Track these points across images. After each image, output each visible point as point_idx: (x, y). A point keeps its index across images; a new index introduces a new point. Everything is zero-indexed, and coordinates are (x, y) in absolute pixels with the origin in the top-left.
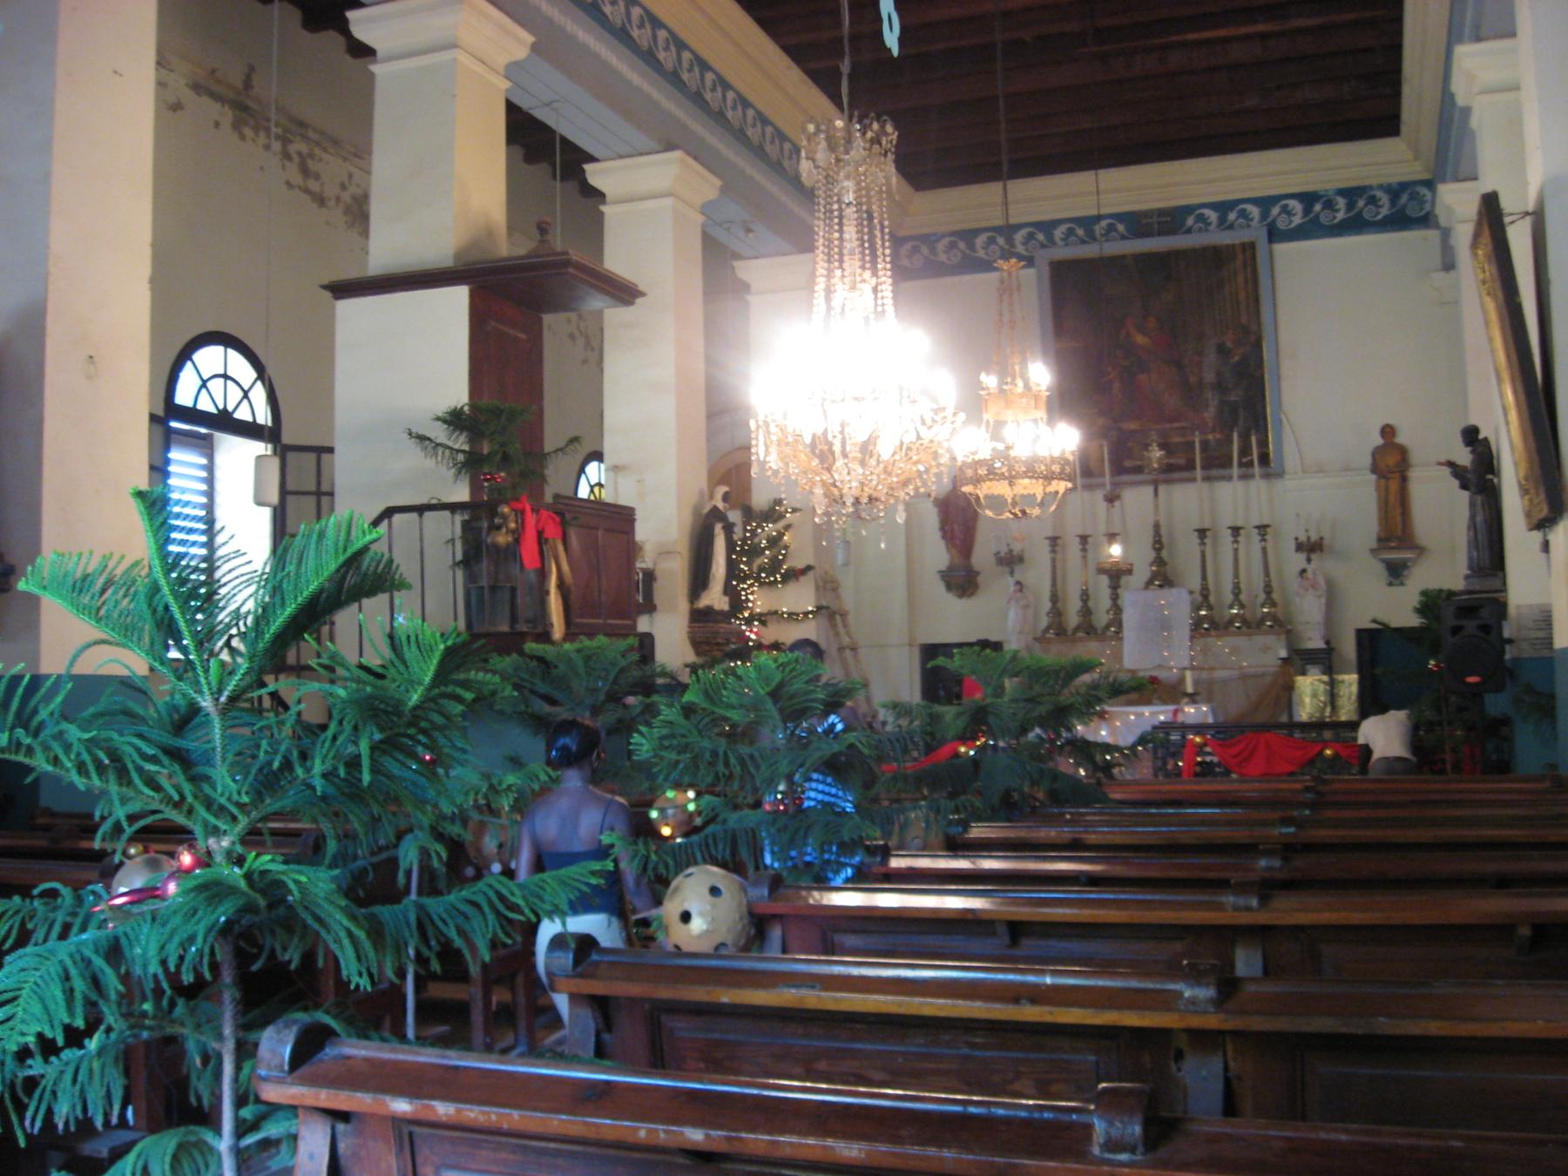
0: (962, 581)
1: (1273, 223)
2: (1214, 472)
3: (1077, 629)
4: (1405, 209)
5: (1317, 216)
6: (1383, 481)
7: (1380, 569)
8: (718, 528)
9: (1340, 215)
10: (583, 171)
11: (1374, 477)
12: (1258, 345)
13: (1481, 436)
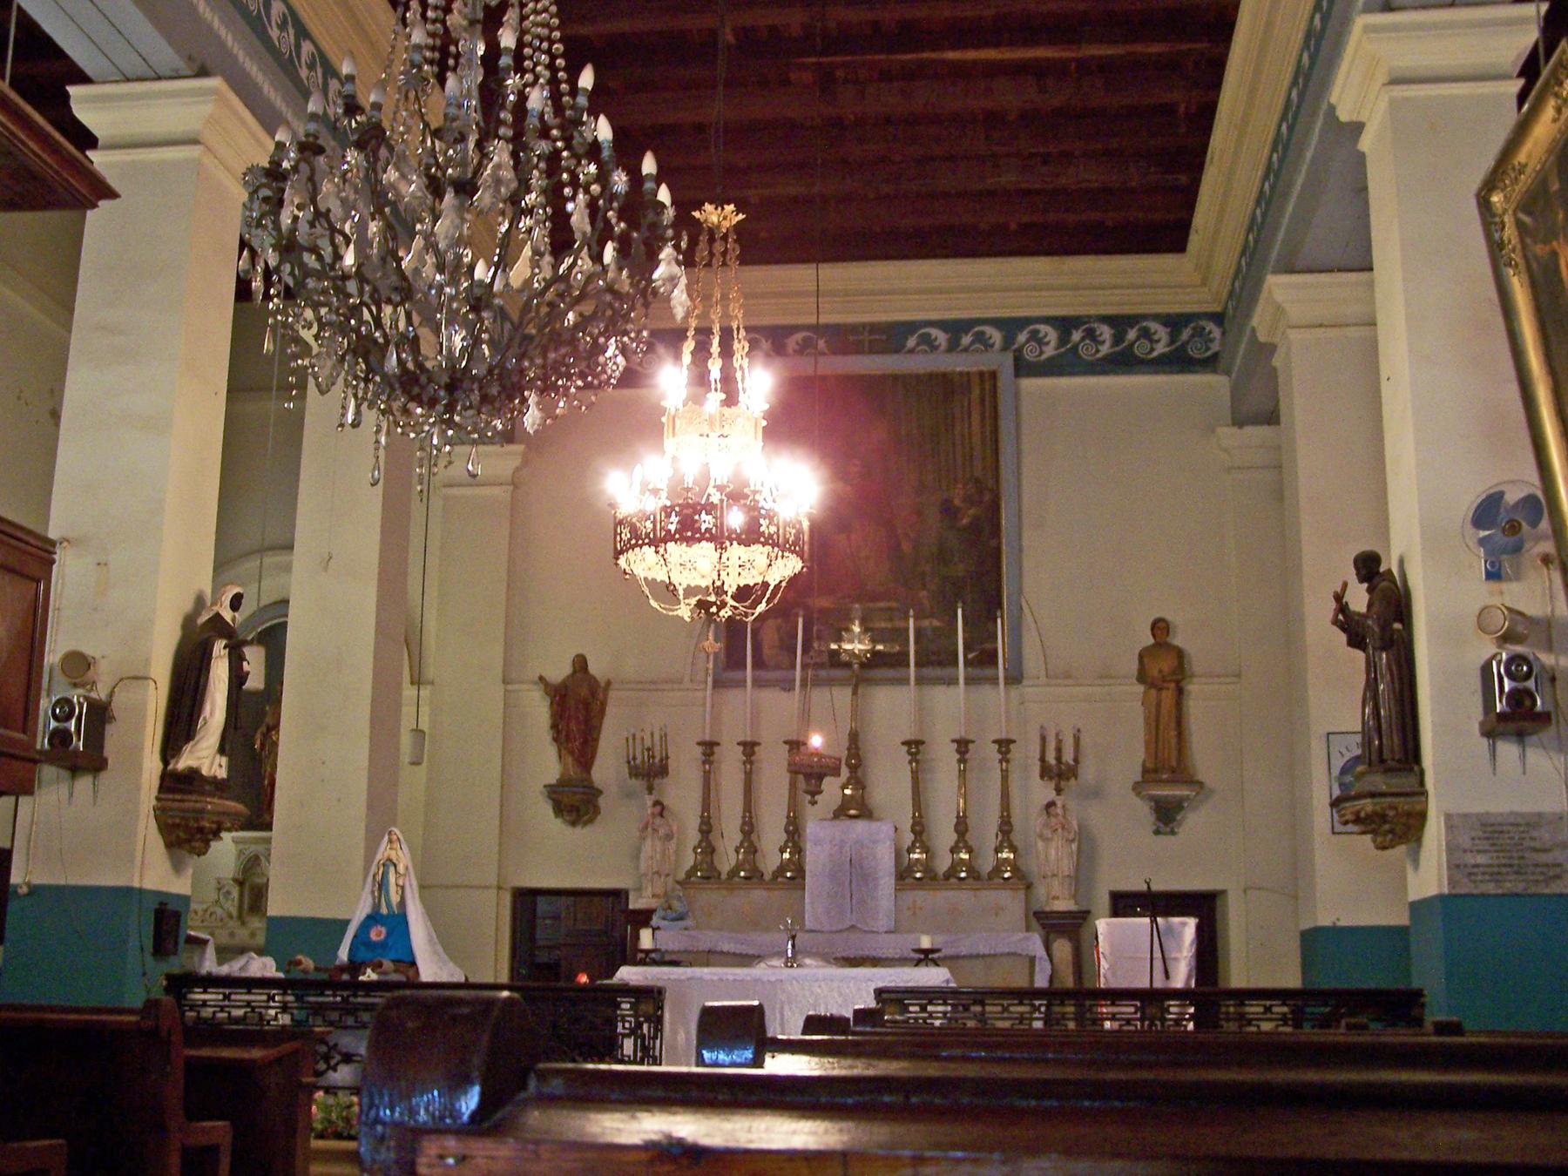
0: (576, 802)
1: (1019, 351)
2: (930, 672)
3: (734, 873)
4: (1187, 344)
5: (1075, 348)
6: (1153, 692)
7: (1144, 810)
8: (219, 648)
9: (1105, 349)
10: (67, 96)
11: (1141, 688)
12: (995, 507)
13: (1366, 585)
